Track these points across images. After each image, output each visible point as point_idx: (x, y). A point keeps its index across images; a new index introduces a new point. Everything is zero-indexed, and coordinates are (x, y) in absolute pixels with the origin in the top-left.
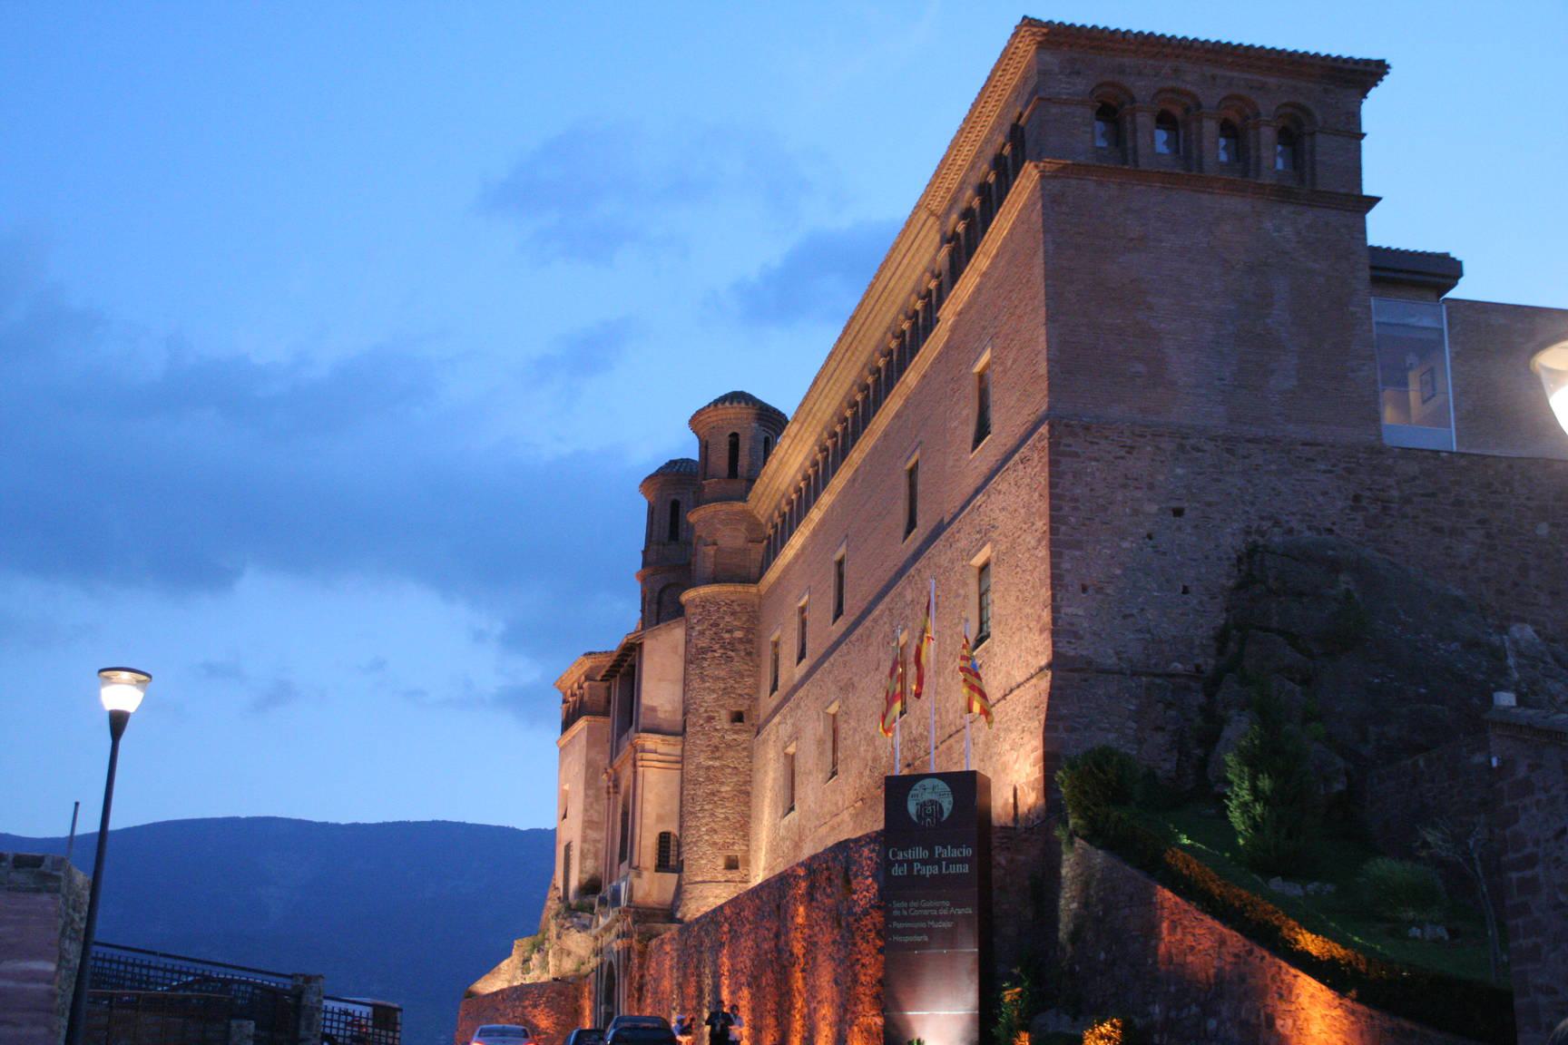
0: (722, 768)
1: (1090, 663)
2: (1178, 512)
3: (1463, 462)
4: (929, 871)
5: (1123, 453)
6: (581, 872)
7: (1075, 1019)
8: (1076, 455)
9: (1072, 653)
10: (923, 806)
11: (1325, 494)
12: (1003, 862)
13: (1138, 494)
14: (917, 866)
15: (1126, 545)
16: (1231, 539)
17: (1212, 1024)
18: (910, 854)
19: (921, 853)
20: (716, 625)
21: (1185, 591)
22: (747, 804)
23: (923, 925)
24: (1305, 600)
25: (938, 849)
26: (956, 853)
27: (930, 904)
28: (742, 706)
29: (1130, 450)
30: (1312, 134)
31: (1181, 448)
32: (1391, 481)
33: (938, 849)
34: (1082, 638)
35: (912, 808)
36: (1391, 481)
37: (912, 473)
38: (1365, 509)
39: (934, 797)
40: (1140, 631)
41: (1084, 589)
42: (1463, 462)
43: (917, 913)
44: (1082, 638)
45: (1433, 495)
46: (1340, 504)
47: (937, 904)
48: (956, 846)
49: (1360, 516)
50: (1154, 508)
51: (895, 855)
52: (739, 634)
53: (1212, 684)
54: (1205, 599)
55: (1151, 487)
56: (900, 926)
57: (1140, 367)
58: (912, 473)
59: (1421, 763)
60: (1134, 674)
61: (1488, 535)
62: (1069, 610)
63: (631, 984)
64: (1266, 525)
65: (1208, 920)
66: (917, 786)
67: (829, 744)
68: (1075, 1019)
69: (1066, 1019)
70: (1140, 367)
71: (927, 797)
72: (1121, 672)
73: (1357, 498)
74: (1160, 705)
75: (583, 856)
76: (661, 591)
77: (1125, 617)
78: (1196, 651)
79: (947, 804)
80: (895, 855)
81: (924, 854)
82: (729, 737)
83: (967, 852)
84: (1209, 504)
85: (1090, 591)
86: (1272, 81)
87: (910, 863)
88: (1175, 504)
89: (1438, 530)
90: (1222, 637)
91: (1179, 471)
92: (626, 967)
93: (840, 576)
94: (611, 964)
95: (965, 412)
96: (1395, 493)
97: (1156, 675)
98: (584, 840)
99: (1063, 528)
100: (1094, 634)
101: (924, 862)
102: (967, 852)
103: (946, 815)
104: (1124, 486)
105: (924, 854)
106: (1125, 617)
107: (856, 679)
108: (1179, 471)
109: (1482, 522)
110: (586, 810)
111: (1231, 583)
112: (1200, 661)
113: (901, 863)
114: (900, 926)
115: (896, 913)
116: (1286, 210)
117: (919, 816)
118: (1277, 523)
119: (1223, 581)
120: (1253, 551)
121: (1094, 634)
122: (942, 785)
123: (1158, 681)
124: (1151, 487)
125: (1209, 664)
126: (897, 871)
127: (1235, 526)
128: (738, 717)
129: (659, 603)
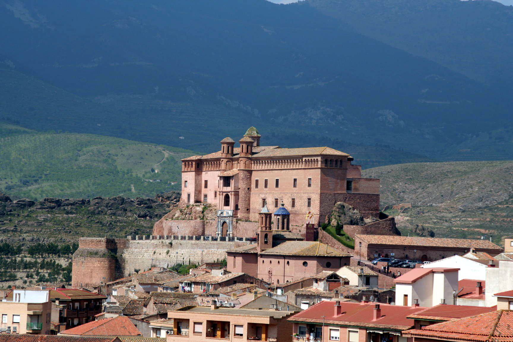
128: (248, 189)
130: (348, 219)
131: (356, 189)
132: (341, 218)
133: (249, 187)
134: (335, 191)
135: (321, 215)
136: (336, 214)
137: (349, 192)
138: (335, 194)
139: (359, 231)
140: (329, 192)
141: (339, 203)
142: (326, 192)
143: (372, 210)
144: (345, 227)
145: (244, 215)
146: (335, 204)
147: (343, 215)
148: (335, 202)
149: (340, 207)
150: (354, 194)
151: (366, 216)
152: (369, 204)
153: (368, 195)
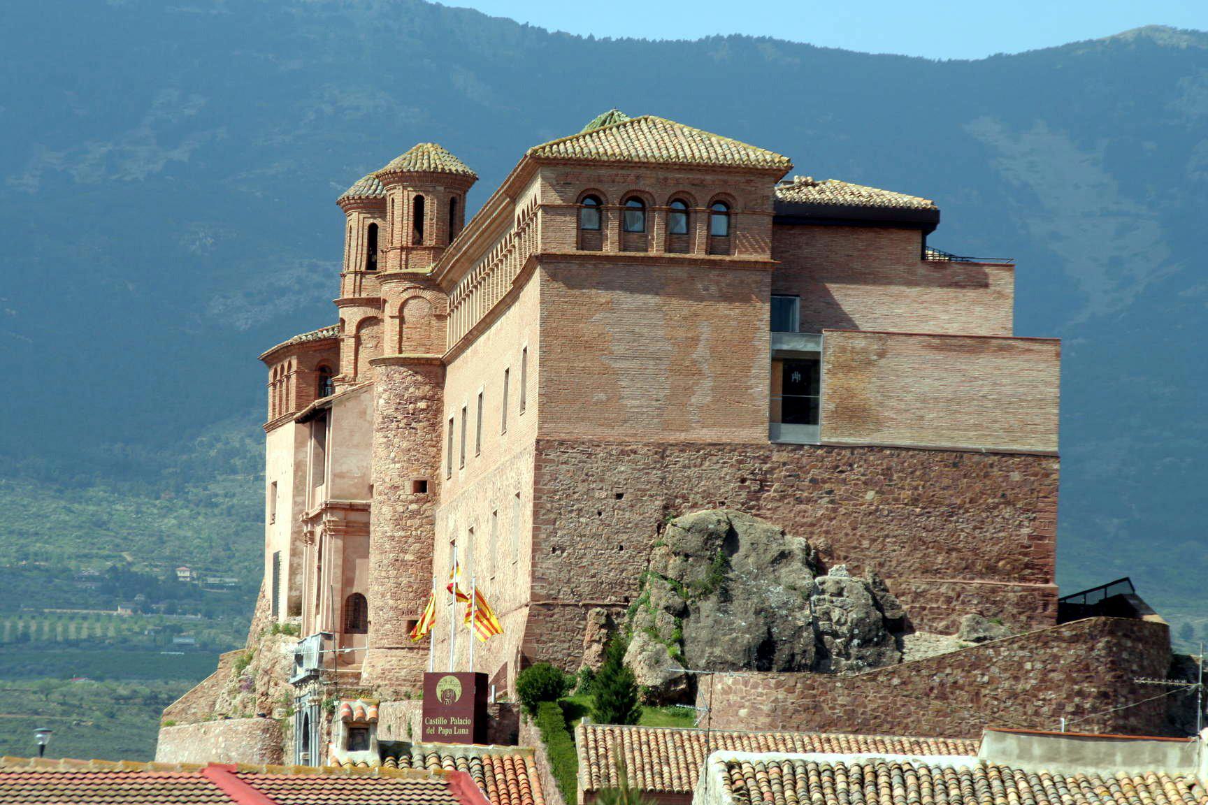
2: (619, 496)
10: (444, 692)
14: (440, 729)
19: (442, 721)
25: (452, 719)
26: (462, 722)
33: (452, 719)
52: (422, 405)
79: (458, 692)
82: (414, 507)
87: (437, 727)
101: (444, 726)
122: (457, 681)
128: (421, 486)
130: (742, 627)
131: (853, 414)
132: (690, 629)
133: (423, 474)
134: (666, 426)
135: (543, 607)
136: (658, 595)
137: (793, 433)
138: (662, 451)
139: (755, 711)
140: (614, 434)
141: (689, 518)
142: (584, 431)
143: (991, 570)
144: (459, 649)
145: (395, 658)
146: (660, 526)
147: (708, 606)
148: (670, 510)
149: (694, 541)
150: (830, 448)
151: (937, 615)
152: (964, 526)
153: (957, 456)
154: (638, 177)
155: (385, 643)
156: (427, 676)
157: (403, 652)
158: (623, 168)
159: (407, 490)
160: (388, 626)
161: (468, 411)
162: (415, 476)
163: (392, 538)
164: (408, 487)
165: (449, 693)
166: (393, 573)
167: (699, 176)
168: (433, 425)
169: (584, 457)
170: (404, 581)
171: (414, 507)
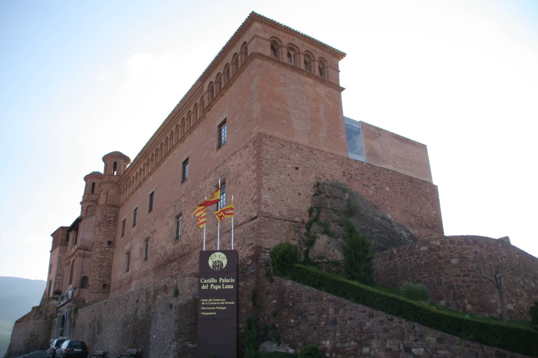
0: (104, 258)
1: (271, 215)
2: (297, 169)
3: (369, 166)
4: (217, 287)
5: (281, 146)
6: (54, 288)
7: (279, 345)
8: (267, 145)
9: (266, 211)
10: (215, 262)
11: (336, 170)
12: (242, 285)
13: (285, 161)
14: (212, 286)
15: (282, 177)
16: (312, 179)
17: (366, 350)
18: (209, 281)
19: (213, 280)
20: (105, 216)
21: (299, 194)
22: (111, 269)
23: (214, 308)
24: (338, 200)
25: (221, 279)
26: (228, 281)
27: (217, 300)
28: (112, 239)
29: (283, 146)
30: (327, 67)
31: (298, 148)
32: (352, 169)
33: (221, 279)
34: (269, 206)
35: (211, 263)
36: (352, 169)
37: (152, 194)
38: (346, 176)
39: (219, 259)
40: (286, 206)
41: (269, 189)
42: (369, 166)
43: (212, 303)
44: (269, 206)
45: (362, 175)
46: (340, 173)
47: (220, 300)
48: (228, 278)
49: (345, 178)
50: (290, 166)
51: (203, 281)
52: (112, 219)
53: (309, 226)
54: (305, 198)
55: (289, 159)
56: (204, 308)
57: (285, 122)
58: (152, 194)
59: (395, 251)
60: (285, 220)
61: (376, 189)
62: (265, 196)
63: (71, 322)
64: (321, 177)
65: (361, 307)
66: (213, 255)
67: (144, 250)
68: (279, 345)
69: (275, 345)
70: (285, 122)
71: (217, 259)
72: (281, 220)
73: (344, 172)
74: (294, 232)
75: (55, 284)
76: (88, 207)
77: (282, 201)
78: (303, 215)
79: (225, 262)
80: (203, 281)
81: (215, 281)
82: (107, 249)
83: (233, 280)
84: (306, 167)
85: (271, 190)
86: (318, 50)
87: (209, 284)
88: (296, 166)
89: (364, 185)
90: (311, 211)
91: (297, 155)
92: (69, 317)
93: (135, 214)
94: (64, 316)
95: (213, 139)
96: (353, 172)
97: (292, 221)
98: (56, 279)
99: (263, 168)
100: (273, 205)
101: (215, 284)
102: (233, 280)
103: (224, 266)
104: (282, 157)
105: (215, 281)
106: (282, 201)
107: (157, 229)
108: (297, 155)
109: (374, 184)
110: (57, 270)
111: (312, 194)
112: (304, 218)
113: (205, 284)
114: (204, 308)
115: (203, 303)
116: (322, 86)
117: (213, 267)
118: (324, 177)
119: (310, 192)
120: (318, 184)
121: (273, 205)
122: (223, 255)
123: (293, 223)
124: (289, 159)
125: (307, 219)
126: (204, 287)
127: (313, 175)
128: (109, 243)
129: (87, 211)
154: (293, 39)
155: (95, 291)
156: (202, 253)
157: (101, 294)
158: (288, 33)
159: (105, 244)
160: (96, 286)
161: (127, 222)
162: (108, 239)
163: (99, 258)
164: (106, 242)
165: (218, 264)
166: (98, 269)
167: (314, 48)
168: (115, 225)
169: (281, 146)
170: (103, 271)
171: (107, 249)
